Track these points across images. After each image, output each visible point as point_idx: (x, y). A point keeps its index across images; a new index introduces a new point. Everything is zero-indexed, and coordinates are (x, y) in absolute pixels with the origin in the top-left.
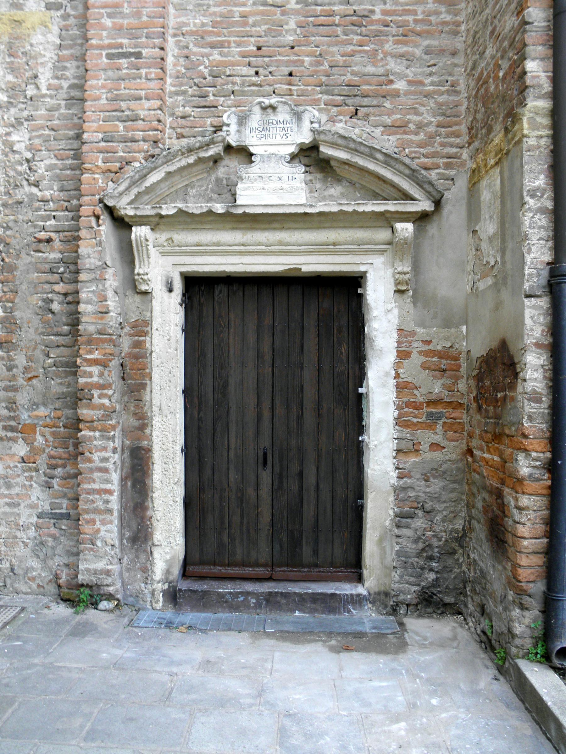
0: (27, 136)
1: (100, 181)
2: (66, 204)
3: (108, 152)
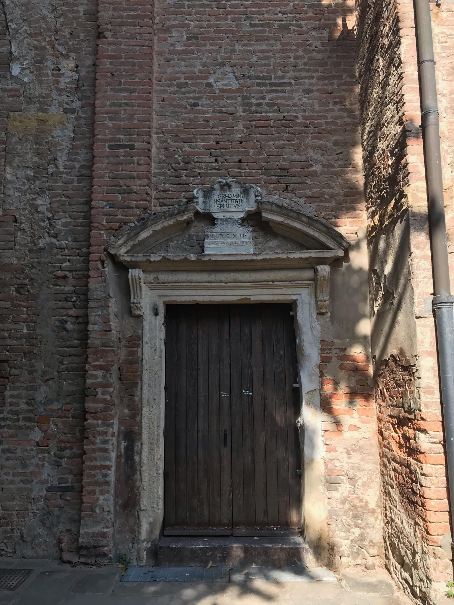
0: (48, 201)
1: (105, 236)
2: (78, 251)
3: (110, 215)
